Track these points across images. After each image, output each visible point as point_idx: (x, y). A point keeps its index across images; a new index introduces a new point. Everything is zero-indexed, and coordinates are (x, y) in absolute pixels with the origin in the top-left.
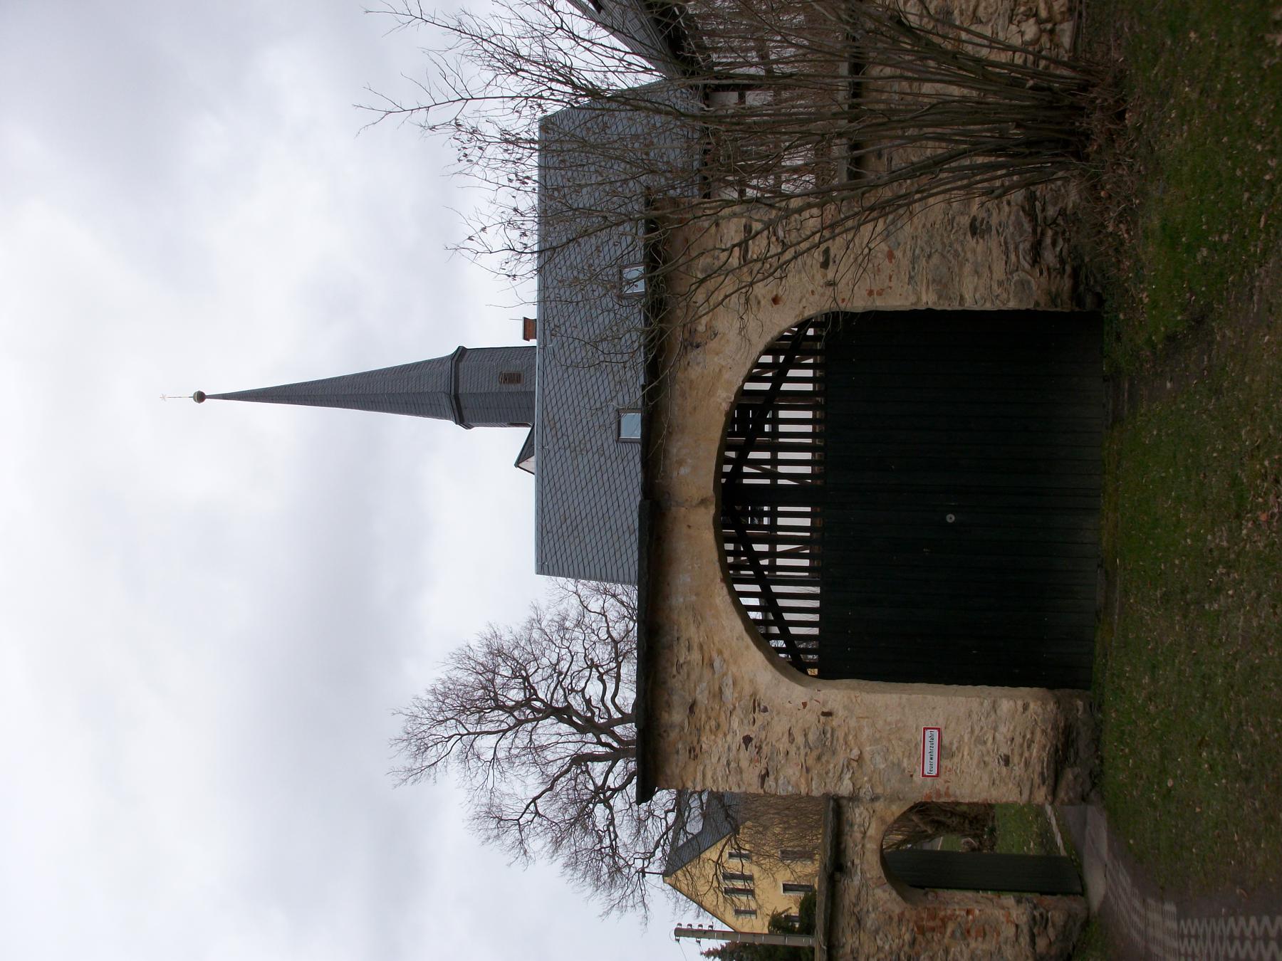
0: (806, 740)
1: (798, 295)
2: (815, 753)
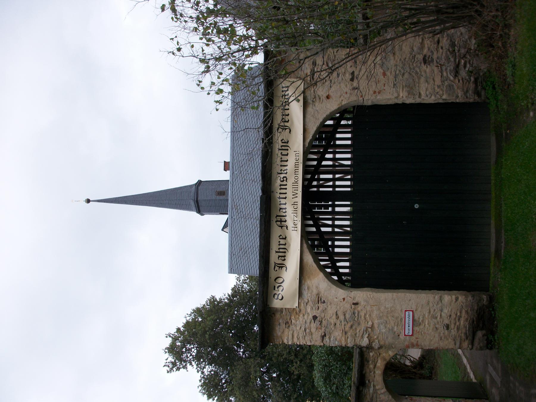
0: (345, 318)
1: (339, 94)
2: (349, 325)
